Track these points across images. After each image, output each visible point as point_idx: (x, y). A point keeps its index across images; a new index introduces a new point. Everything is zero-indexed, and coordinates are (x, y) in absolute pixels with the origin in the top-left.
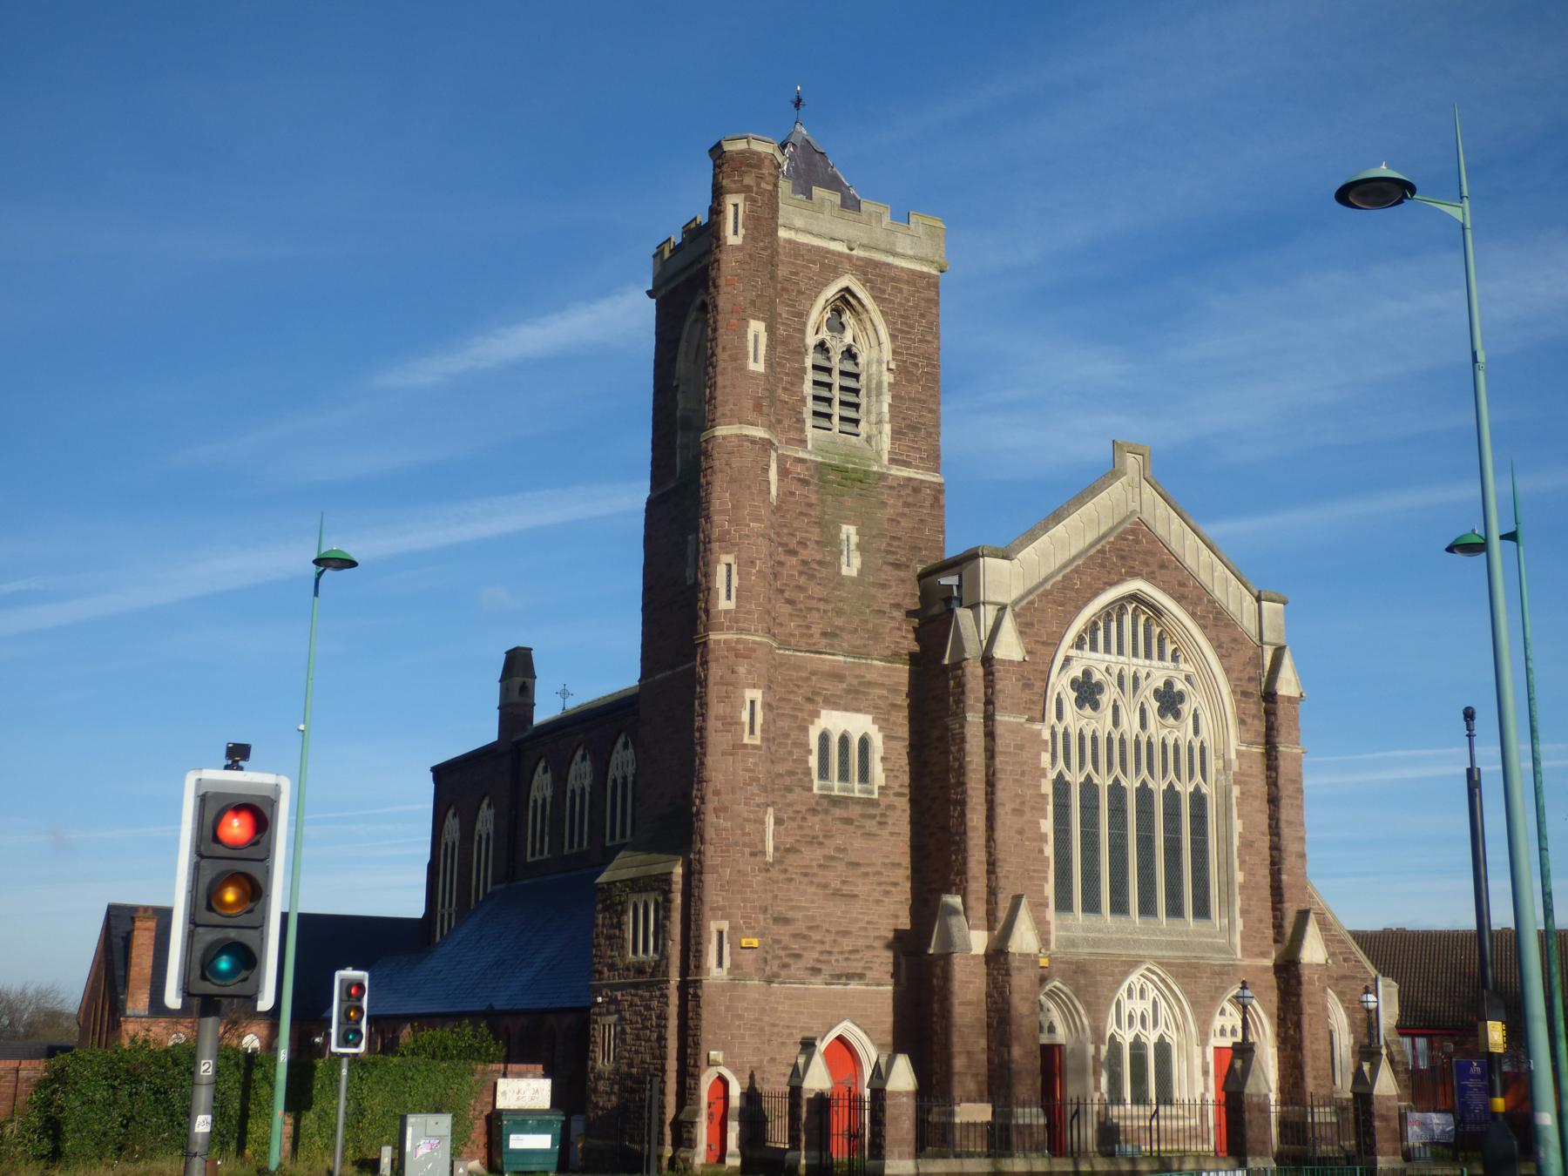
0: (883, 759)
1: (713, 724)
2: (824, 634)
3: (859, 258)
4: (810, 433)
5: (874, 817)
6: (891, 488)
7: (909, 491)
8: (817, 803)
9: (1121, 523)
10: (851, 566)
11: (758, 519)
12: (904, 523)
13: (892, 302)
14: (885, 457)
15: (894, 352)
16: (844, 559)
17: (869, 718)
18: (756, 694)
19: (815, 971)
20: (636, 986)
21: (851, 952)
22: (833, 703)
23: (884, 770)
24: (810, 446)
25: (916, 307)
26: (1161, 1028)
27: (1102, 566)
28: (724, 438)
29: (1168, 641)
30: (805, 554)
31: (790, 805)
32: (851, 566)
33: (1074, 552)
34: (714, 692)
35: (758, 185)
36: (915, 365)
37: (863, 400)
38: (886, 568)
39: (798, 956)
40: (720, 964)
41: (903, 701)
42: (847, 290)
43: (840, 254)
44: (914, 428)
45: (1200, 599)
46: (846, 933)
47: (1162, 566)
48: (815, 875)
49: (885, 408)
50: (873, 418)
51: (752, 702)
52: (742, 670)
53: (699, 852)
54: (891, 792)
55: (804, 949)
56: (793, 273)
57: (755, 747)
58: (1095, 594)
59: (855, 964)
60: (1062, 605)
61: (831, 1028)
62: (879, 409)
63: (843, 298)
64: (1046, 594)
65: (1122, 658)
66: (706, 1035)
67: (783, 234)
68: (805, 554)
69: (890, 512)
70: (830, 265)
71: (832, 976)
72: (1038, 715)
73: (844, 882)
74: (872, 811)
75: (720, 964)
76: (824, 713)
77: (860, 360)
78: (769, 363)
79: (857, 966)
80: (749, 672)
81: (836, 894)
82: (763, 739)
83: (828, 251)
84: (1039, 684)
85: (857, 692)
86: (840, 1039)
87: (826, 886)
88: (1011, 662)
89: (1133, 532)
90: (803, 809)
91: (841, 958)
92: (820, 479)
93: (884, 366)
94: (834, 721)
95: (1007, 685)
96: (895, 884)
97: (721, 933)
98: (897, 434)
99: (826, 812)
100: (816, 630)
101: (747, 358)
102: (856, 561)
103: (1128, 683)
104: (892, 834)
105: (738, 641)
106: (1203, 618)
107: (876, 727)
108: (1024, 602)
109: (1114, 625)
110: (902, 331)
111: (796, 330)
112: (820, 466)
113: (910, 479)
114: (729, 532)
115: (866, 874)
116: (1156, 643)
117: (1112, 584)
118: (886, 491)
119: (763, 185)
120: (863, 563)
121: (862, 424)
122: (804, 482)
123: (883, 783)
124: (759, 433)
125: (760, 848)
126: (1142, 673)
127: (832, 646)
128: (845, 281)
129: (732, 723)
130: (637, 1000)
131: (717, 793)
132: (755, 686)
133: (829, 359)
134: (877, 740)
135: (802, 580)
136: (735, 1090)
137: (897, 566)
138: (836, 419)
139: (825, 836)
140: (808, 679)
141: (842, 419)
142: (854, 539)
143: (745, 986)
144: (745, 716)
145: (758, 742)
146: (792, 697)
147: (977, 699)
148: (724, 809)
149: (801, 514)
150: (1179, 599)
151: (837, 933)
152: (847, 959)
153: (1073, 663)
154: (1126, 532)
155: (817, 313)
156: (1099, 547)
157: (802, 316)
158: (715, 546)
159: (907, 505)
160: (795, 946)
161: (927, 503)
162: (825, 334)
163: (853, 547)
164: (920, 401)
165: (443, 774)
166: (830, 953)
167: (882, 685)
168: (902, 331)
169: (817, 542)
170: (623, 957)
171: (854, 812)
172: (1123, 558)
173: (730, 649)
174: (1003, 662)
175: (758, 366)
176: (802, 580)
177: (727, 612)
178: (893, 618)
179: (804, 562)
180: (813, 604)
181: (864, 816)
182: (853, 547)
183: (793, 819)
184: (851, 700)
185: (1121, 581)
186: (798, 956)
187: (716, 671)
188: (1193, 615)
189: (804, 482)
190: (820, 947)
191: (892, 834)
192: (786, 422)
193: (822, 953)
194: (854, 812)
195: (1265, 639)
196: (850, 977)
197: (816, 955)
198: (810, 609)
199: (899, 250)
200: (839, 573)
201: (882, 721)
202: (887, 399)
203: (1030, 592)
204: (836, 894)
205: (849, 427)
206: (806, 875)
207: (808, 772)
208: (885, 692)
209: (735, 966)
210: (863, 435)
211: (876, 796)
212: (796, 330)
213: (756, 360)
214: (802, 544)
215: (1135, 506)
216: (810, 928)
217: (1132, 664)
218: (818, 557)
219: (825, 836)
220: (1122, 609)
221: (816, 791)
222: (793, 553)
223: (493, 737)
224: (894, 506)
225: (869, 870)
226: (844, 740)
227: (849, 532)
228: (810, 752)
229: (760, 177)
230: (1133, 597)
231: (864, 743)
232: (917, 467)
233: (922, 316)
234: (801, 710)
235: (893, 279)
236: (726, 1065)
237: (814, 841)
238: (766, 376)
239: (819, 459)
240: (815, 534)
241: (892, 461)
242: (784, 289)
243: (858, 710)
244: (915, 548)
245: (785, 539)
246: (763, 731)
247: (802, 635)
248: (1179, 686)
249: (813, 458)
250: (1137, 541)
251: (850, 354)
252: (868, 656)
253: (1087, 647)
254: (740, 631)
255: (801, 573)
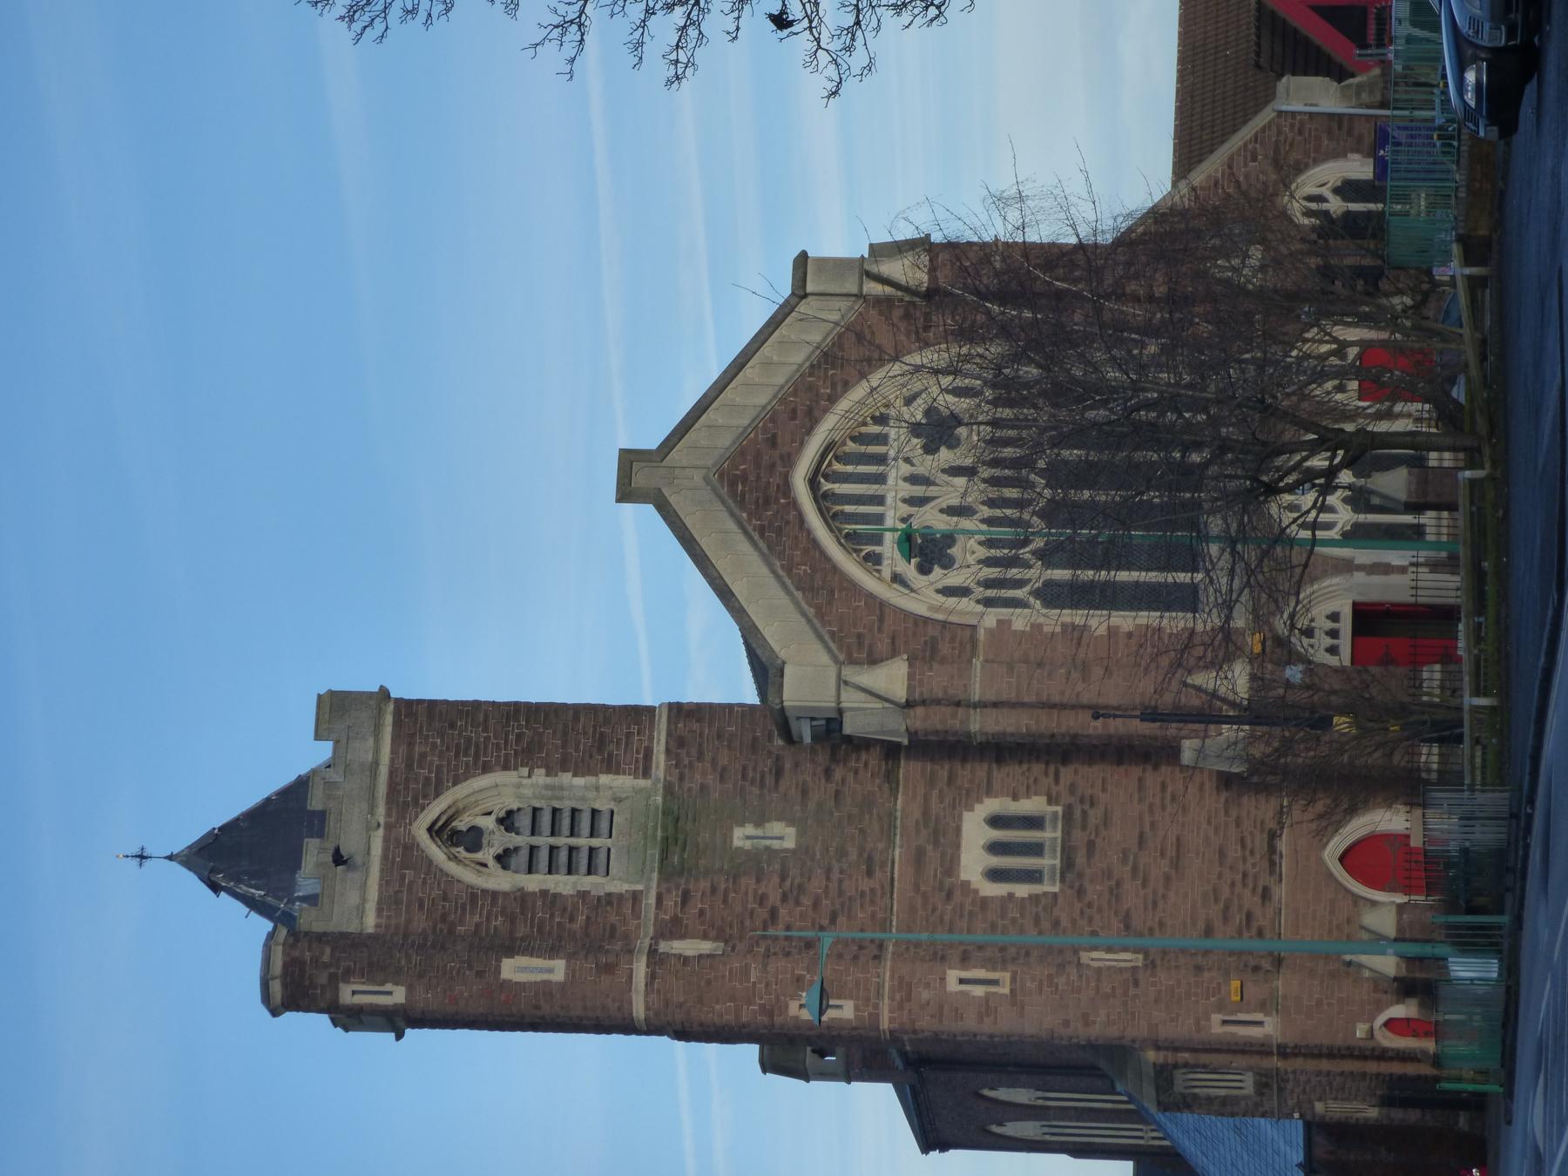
0: (1015, 798)
1: (987, 1027)
2: (870, 873)
3: (388, 814)
4: (616, 885)
5: (1084, 813)
6: (681, 778)
7: (683, 752)
8: (1072, 887)
9: (723, 502)
10: (783, 835)
11: (746, 971)
12: (724, 760)
13: (439, 768)
14: (642, 783)
15: (506, 768)
16: (776, 844)
17: (967, 815)
18: (953, 975)
19: (1266, 894)
20: (1281, 1090)
21: (1243, 846)
22: (951, 864)
23: (1028, 796)
24: (639, 887)
25: (442, 735)
26: (1326, 192)
27: (779, 532)
28: (647, 1008)
29: (863, 429)
30: (774, 898)
31: (1074, 922)
32: (783, 835)
33: (765, 570)
34: (949, 1025)
35: (326, 966)
36: (519, 737)
37: (566, 805)
38: (782, 789)
39: (1249, 916)
40: (1260, 1023)
41: (943, 772)
42: (430, 830)
43: (386, 840)
44: (601, 742)
45: (811, 387)
46: (1222, 854)
47: (773, 442)
48: (1155, 892)
49: (580, 781)
50: (591, 795)
51: (962, 981)
52: (925, 995)
53: (1133, 1041)
54: (1054, 789)
55: (1240, 907)
56: (421, 906)
57: (1013, 980)
58: (815, 543)
59: (1257, 842)
60: (832, 592)
61: (1330, 875)
62: (576, 787)
63: (439, 832)
64: (820, 614)
65: (889, 500)
66: (1339, 1041)
67: (370, 922)
68: (774, 898)
69: (711, 779)
70: (402, 856)
71: (1272, 873)
72: (968, 633)
73: (1162, 854)
74: (1078, 814)
75: (1260, 1023)
76: (963, 876)
77: (514, 807)
78: (552, 953)
79: (1260, 842)
80: (928, 985)
81: (1176, 864)
82: (1004, 969)
83: (385, 857)
84: (932, 631)
85: (936, 832)
86: (1341, 859)
87: (1168, 879)
88: (911, 677)
89: (732, 484)
90: (1078, 905)
91: (1250, 861)
92: (681, 874)
93: (525, 781)
94: (973, 863)
95: (938, 680)
96: (1164, 787)
97: (1225, 1022)
98: (611, 767)
99: (1080, 875)
100: (866, 885)
101: (547, 983)
102: (777, 828)
103: (919, 491)
104: (1104, 789)
105: (892, 998)
106: (833, 386)
107: (978, 807)
108: (833, 646)
109: (849, 508)
110: (477, 756)
111: (494, 903)
112: (667, 874)
113: (668, 751)
114: (762, 1007)
115: (1153, 825)
116: (864, 447)
117: (801, 519)
118: (687, 785)
119: (326, 958)
120: (779, 819)
121: (597, 806)
122: (686, 897)
123: (1044, 799)
124: (640, 969)
125: (1128, 975)
126: (906, 469)
127: (883, 865)
128: (420, 830)
129: (987, 1007)
130: (1298, 1090)
131: (1066, 1023)
132: (943, 979)
133: (517, 849)
134: (992, 805)
135: (807, 901)
136: (1399, 1011)
137: (779, 773)
138: (595, 842)
139: (1110, 877)
140: (925, 896)
141: (593, 833)
142: (750, 830)
143: (1285, 997)
144: (978, 991)
145: (1007, 976)
146: (947, 918)
147: (954, 716)
148: (1085, 1017)
149: (725, 901)
150: (812, 421)
151: (1221, 864)
152: (1252, 853)
153: (899, 569)
154: (733, 493)
155: (462, 872)
156: (756, 536)
157: (475, 896)
158: (778, 1020)
159: (700, 757)
160: (1238, 918)
161: (696, 726)
162: (487, 855)
163: (759, 832)
164: (565, 734)
165: (931, 1138)
166: (1245, 875)
167: (926, 798)
168: (477, 756)
169: (758, 880)
170: (1245, 1097)
171: (1079, 837)
172: (767, 502)
173: (901, 1007)
174: (910, 688)
175: (557, 970)
176: (807, 901)
177: (857, 1008)
178: (843, 781)
179: (784, 898)
180: (833, 886)
181: (1084, 828)
182: (759, 832)
183: (1090, 920)
184: (946, 839)
185: (794, 504)
186: (1249, 916)
187: (926, 1023)
188: (833, 399)
189: (686, 897)
190: (1238, 888)
191: (1104, 789)
192: (613, 919)
193: (1244, 885)
194: (1079, 837)
195: (855, 290)
196: (1272, 849)
197: (1247, 893)
198: (841, 893)
199: (370, 758)
200: (794, 852)
201: (969, 798)
202: (566, 778)
203: (820, 638)
204: (1176, 864)
205: (604, 824)
206: (1155, 904)
207: (1034, 898)
208: (935, 793)
209: (1262, 1006)
210: (612, 805)
211: (1059, 809)
212: (494, 903)
213: (550, 971)
214: (762, 900)
215: (698, 477)
216: (1216, 900)
217: (896, 488)
218: (776, 879)
219: (1110, 877)
220: (827, 496)
221: (1056, 889)
222: (774, 913)
223: (890, 1086)
224: (704, 774)
225: (1147, 819)
226: (995, 848)
227: (742, 836)
228: (1011, 895)
229: (316, 961)
230: (813, 483)
231: (996, 821)
232: (651, 738)
233: (452, 726)
234: (962, 905)
235: (409, 766)
236: (1372, 1019)
237: (1116, 892)
238: (570, 957)
239: (655, 875)
240: (747, 882)
241: (646, 773)
242: (444, 917)
243: (958, 830)
244: (754, 746)
245: (758, 923)
246: (994, 969)
247: (872, 903)
248: (917, 413)
249: (654, 884)
250: (744, 478)
251: (507, 821)
252: (891, 815)
253: (877, 549)
254: (879, 995)
255: (798, 903)
